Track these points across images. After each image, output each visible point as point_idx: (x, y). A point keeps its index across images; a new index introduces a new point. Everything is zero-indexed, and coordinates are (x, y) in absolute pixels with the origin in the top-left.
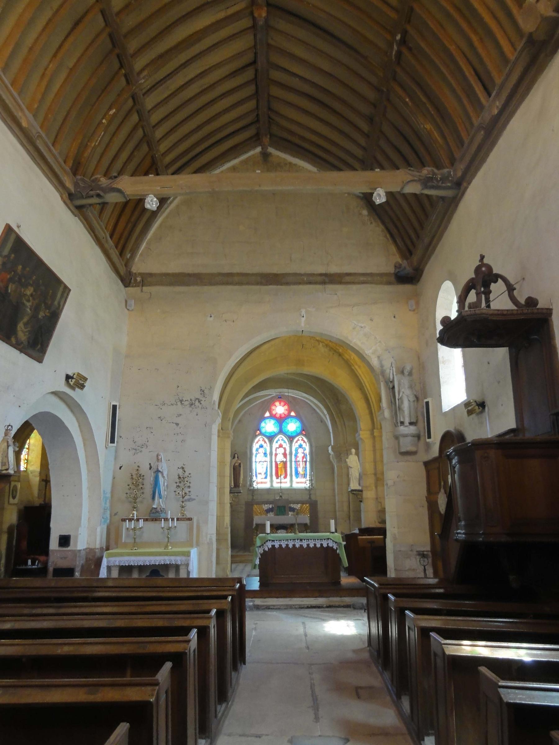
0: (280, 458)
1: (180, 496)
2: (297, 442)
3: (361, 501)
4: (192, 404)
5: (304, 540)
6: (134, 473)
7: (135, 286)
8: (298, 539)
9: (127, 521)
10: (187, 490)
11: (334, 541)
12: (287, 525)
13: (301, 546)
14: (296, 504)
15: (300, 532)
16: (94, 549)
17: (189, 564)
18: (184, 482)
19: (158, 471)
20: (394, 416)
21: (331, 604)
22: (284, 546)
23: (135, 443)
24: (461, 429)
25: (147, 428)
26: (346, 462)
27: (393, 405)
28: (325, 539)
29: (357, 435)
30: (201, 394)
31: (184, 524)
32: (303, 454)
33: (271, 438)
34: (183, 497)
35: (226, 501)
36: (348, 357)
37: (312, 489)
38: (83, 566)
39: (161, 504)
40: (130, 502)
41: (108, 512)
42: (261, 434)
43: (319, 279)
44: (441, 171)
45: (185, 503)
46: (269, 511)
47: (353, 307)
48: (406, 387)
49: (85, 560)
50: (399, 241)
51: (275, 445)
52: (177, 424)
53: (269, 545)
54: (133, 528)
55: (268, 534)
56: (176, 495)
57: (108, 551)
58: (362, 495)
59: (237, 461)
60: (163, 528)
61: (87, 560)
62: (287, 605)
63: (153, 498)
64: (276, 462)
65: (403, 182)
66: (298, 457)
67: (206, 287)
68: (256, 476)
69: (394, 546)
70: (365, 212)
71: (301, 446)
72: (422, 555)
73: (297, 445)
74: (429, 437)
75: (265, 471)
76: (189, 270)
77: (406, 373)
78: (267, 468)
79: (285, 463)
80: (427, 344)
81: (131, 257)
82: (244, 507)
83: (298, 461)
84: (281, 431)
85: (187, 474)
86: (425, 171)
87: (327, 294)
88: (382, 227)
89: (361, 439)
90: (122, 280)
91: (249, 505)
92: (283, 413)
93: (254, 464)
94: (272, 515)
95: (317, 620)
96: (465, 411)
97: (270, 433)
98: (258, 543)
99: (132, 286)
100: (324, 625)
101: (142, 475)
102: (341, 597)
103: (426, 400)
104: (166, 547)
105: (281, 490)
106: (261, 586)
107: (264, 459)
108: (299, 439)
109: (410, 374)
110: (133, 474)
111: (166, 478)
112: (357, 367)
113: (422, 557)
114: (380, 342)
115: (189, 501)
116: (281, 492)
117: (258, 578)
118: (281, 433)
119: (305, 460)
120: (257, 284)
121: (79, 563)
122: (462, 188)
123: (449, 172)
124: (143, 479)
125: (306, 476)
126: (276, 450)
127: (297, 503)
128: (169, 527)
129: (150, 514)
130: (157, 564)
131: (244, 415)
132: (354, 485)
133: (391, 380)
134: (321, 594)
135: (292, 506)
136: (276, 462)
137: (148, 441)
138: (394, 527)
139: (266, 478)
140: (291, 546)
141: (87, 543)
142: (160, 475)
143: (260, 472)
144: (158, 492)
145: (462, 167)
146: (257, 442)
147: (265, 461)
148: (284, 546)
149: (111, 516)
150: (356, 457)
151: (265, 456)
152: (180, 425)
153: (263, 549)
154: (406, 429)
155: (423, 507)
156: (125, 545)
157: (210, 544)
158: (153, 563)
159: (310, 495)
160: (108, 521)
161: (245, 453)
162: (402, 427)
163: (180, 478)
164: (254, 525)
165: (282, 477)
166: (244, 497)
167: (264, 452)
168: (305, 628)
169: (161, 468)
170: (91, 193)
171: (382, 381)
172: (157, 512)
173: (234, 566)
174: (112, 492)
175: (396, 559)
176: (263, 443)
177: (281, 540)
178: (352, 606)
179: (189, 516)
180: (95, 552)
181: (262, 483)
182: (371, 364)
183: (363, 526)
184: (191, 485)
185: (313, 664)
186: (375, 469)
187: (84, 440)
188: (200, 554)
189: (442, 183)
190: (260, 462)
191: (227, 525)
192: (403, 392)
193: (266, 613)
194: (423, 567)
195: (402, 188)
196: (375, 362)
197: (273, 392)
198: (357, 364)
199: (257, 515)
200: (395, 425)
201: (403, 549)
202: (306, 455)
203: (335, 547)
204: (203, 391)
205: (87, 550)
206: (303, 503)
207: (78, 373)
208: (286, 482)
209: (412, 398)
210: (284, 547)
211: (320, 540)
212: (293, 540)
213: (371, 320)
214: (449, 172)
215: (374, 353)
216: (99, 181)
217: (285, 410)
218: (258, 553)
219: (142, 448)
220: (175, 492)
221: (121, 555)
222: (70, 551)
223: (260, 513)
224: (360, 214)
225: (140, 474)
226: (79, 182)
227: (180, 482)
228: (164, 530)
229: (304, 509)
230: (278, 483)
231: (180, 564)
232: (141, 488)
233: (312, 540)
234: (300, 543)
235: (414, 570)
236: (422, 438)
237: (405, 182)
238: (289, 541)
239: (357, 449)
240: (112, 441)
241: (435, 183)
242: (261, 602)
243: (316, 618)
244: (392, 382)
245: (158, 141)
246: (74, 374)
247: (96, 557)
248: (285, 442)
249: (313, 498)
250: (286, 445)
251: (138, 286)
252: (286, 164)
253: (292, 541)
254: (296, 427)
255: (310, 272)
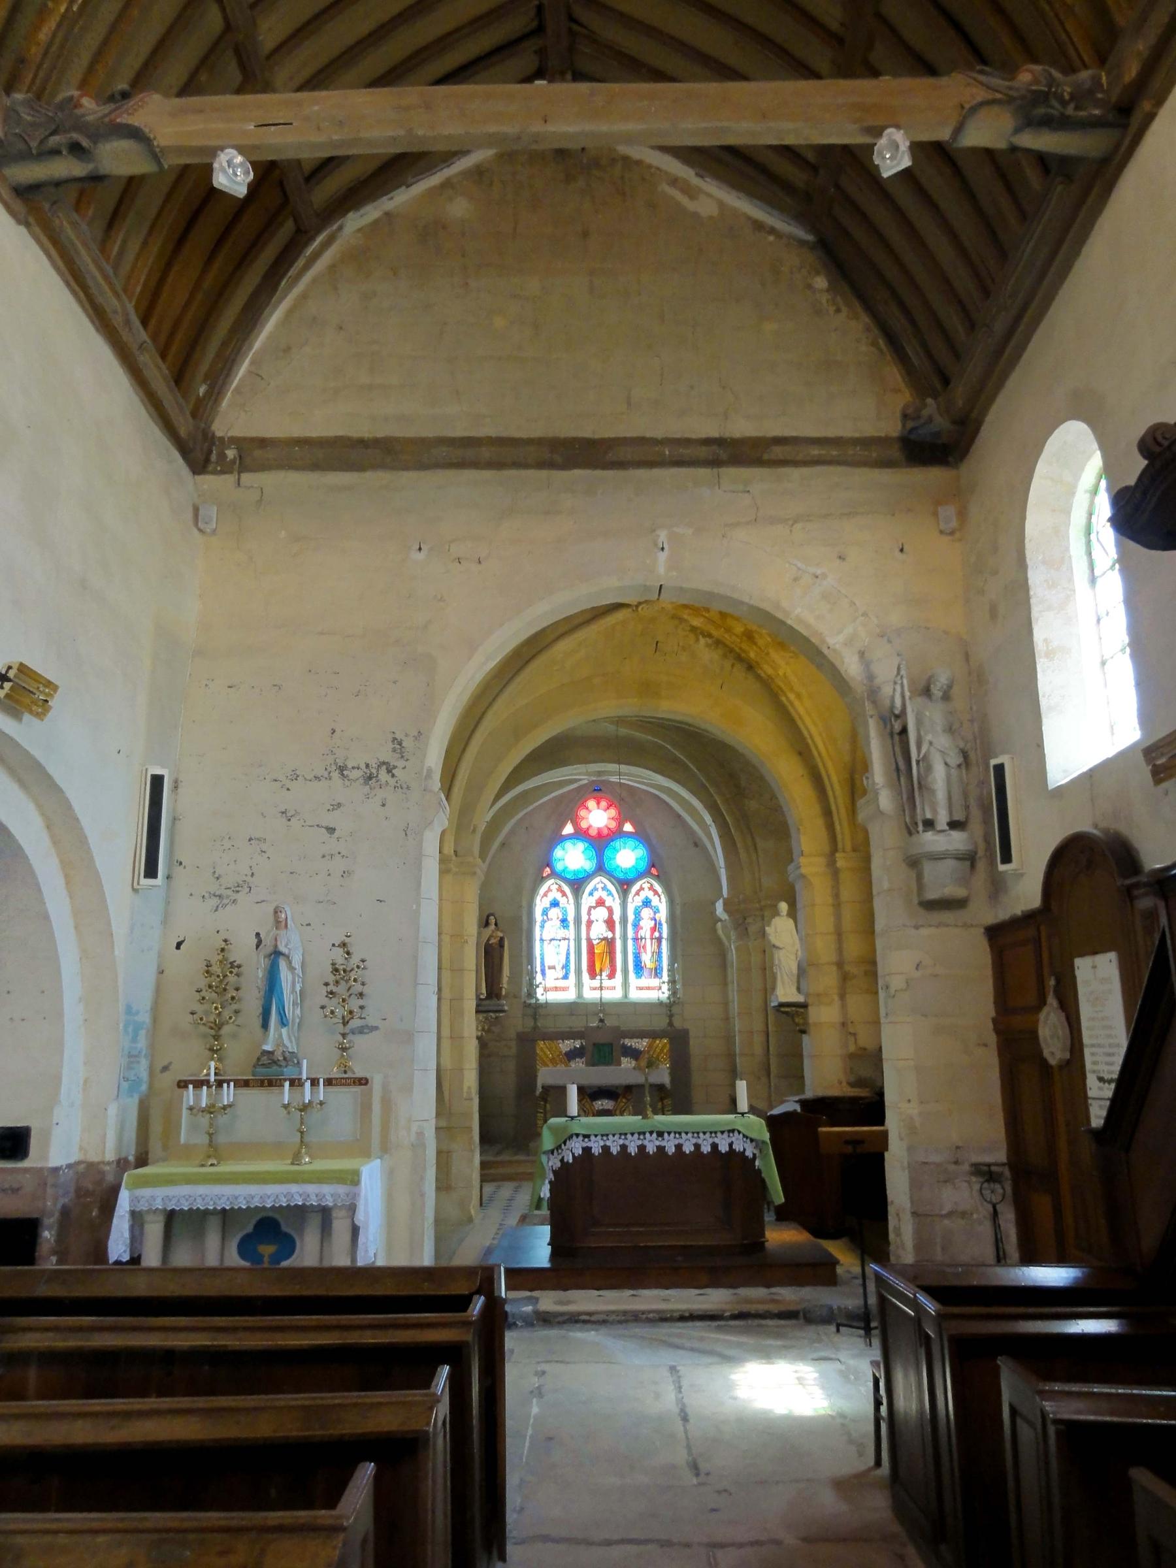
0: (599, 931)
1: (335, 1020)
2: (637, 893)
3: (803, 1032)
4: (370, 778)
5: (669, 1133)
6: (215, 958)
7: (222, 472)
8: (651, 1133)
9: (191, 1087)
10: (354, 1003)
11: (747, 1138)
12: (617, 1087)
13: (661, 1149)
14: (637, 1038)
15: (655, 1112)
16: (99, 1163)
17: (355, 1205)
18: (347, 981)
19: (276, 954)
20: (906, 807)
21: (746, 1308)
22: (615, 1150)
23: (218, 878)
24: (1123, 829)
25: (250, 840)
26: (763, 934)
27: (903, 780)
28: (722, 1132)
29: (791, 867)
30: (394, 750)
31: (344, 1097)
32: (653, 922)
33: (577, 885)
34: (345, 1023)
35: (466, 1034)
36: (770, 671)
37: (674, 1002)
38: (65, 1213)
39: (286, 1042)
40: (205, 1036)
41: (144, 1063)
42: (554, 874)
43: (703, 452)
44: (1072, 78)
45: (350, 1037)
46: (572, 1055)
47: (792, 525)
48: (939, 728)
49: (72, 1195)
50: (912, 349)
51: (587, 901)
52: (331, 830)
53: (577, 1147)
54: (204, 1106)
55: (572, 1118)
56: (326, 1016)
57: (140, 1171)
58: (805, 1017)
59: (493, 932)
60: (286, 1107)
61: (81, 1193)
62: (625, 1313)
63: (265, 1025)
64: (589, 941)
65: (962, 107)
66: (642, 928)
67: (405, 473)
68: (543, 973)
69: (911, 1149)
70: (821, 282)
71: (647, 903)
72: (987, 1174)
73: (638, 901)
74: (1007, 858)
75: (563, 961)
76: (362, 429)
77: (937, 692)
78: (568, 954)
79: (610, 943)
80: (993, 613)
81: (209, 393)
82: (513, 1044)
83: (642, 939)
84: (601, 869)
85: (355, 960)
86: (1027, 76)
87: (725, 491)
88: (866, 319)
89: (803, 876)
90: (184, 448)
91: (527, 1041)
92: (606, 826)
93: (537, 945)
94: (581, 1064)
95: (709, 1360)
96: (1146, 770)
97: (575, 872)
98: (547, 1141)
99: (215, 472)
100: (733, 1377)
101: (235, 964)
102: (768, 1286)
103: (993, 762)
104: (296, 1159)
105: (602, 1007)
106: (554, 1256)
107: (562, 933)
108: (644, 886)
109: (946, 697)
110: (213, 962)
111: (299, 971)
112: (792, 696)
113: (988, 1181)
114: (865, 614)
115: (361, 1032)
116: (601, 1011)
117: (546, 1230)
118: (602, 873)
119: (657, 934)
120: (541, 465)
121: (50, 1207)
122: (1136, 119)
123: (1096, 81)
124: (238, 975)
125: (661, 973)
126: (589, 913)
127: (641, 1035)
128: (304, 1103)
129: (254, 1066)
130: (268, 1206)
131: (512, 832)
132: (786, 992)
133: (897, 712)
134: (715, 1278)
135: (628, 1042)
136: (589, 941)
137: (253, 875)
138: (909, 1101)
139: (566, 977)
140: (633, 1150)
141: (81, 1148)
142: (282, 964)
143: (551, 964)
144: (278, 1009)
145: (1141, 48)
146: (545, 895)
147: (564, 939)
148: (615, 1150)
149: (151, 1074)
150: (791, 922)
151: (564, 927)
152: (337, 834)
153: (560, 1157)
154: (940, 838)
155: (986, 1045)
156: (186, 1153)
157: (418, 1145)
158: (256, 1203)
159: (671, 1016)
160: (144, 1087)
161: (517, 919)
162: (930, 833)
163: (337, 970)
164: (539, 1090)
165: (604, 974)
166: (516, 1023)
167: (561, 917)
168: (680, 1387)
169: (286, 946)
170: (54, 140)
171: (871, 717)
172: (275, 1062)
173: (489, 1188)
174: (156, 1010)
175: (915, 1184)
176: (558, 896)
177: (607, 1135)
178: (801, 1314)
179: (359, 1073)
180: (103, 1173)
181: (556, 989)
182: (843, 672)
183: (809, 1094)
184: (366, 990)
185: (722, 1546)
186: (840, 950)
187: (66, 866)
188: (390, 1175)
189: (1077, 108)
190: (551, 940)
191: (469, 1093)
192: (931, 743)
193: (571, 1334)
194: (991, 1209)
195: (958, 130)
196: (851, 667)
197: (579, 773)
198: (792, 690)
199: (546, 1065)
200: (908, 828)
201: (935, 1158)
202: (660, 924)
203: (749, 1154)
204: (400, 744)
205: (81, 1168)
206: (653, 1035)
207: (21, 664)
208: (614, 988)
209: (955, 759)
210: (615, 1153)
211: (711, 1133)
212: (639, 1134)
213: (841, 558)
214: (1096, 81)
215: (849, 643)
216: (78, 105)
217: (609, 818)
218: (547, 1168)
219: (238, 892)
220: (323, 1007)
221: (170, 1181)
222: (26, 1170)
223: (554, 1061)
224: (809, 287)
225: (232, 960)
226: (21, 109)
227: (337, 982)
228: (289, 1113)
229: (658, 1050)
230: (595, 989)
231: (331, 1204)
232: (233, 998)
233: (690, 1135)
234: (658, 1143)
235: (963, 1215)
236: (981, 865)
237: (967, 106)
238: (629, 1136)
239: (793, 905)
240: (151, 870)
241: (1055, 109)
242: (556, 1303)
243: (711, 1353)
244: (901, 716)
245: (268, 57)
246: (10, 668)
247: (105, 1185)
248: (610, 894)
249: (678, 1023)
250: (614, 902)
251: (231, 473)
252: (613, 161)
253: (636, 1136)
254: (637, 859)
255: (678, 436)
